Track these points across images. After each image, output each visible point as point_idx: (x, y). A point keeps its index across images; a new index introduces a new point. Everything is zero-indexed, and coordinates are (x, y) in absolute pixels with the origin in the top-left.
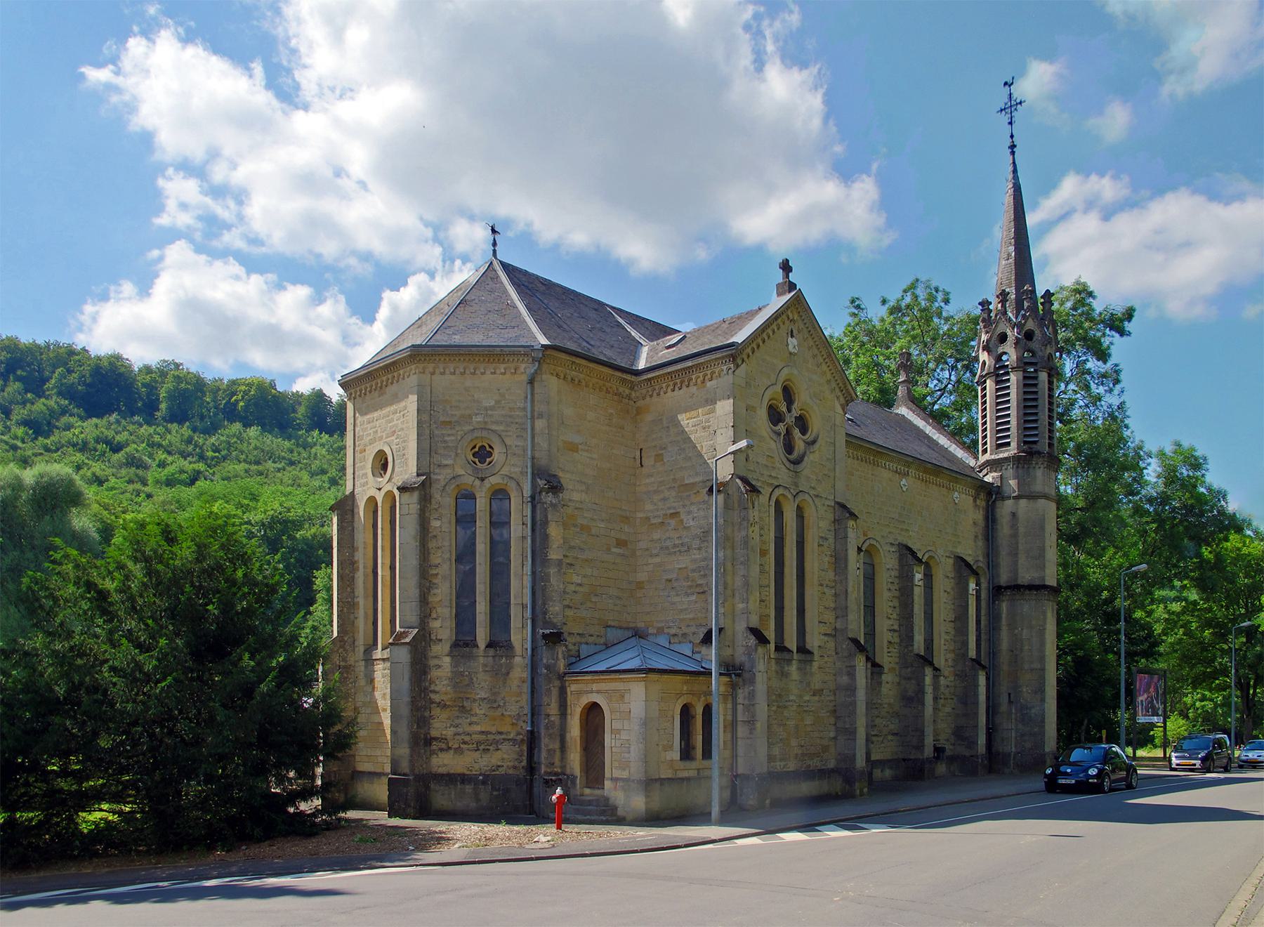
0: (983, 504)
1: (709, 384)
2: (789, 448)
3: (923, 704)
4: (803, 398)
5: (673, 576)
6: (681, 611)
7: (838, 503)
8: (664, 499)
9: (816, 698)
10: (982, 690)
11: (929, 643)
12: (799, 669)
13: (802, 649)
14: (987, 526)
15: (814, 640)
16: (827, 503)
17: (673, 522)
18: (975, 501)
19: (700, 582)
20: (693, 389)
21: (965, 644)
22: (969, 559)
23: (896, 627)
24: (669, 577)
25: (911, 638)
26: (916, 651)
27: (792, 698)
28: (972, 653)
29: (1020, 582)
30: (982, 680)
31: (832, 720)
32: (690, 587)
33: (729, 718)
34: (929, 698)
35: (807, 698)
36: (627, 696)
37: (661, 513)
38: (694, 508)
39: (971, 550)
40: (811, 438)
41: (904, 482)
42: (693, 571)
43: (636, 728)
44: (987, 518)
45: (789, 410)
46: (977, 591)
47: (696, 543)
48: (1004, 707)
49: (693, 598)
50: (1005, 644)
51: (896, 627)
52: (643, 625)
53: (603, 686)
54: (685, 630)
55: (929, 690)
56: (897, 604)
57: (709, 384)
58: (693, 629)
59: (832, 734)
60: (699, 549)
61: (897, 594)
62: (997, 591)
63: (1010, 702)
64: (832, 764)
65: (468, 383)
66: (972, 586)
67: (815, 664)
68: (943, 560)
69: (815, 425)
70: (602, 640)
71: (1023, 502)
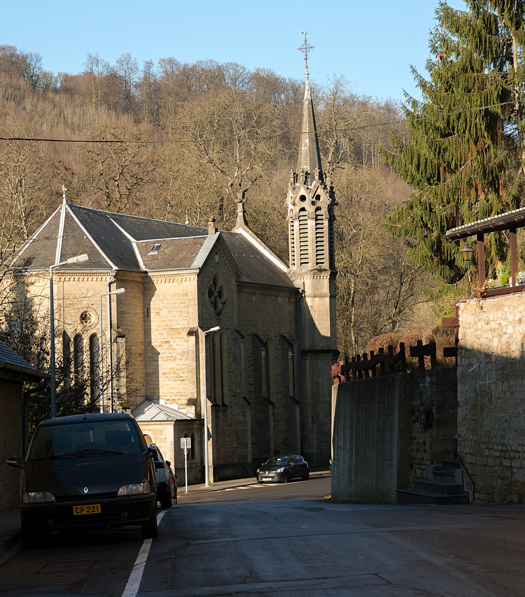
0: (294, 300)
1: (184, 283)
2: (215, 308)
3: (269, 427)
4: (221, 282)
5: (167, 371)
6: (172, 388)
7: (236, 330)
8: (161, 334)
9: (229, 428)
10: (298, 416)
11: (268, 391)
12: (223, 414)
13: (224, 405)
14: (296, 314)
15: (227, 402)
16: (231, 331)
17: (166, 346)
18: (289, 300)
19: (181, 375)
20: (176, 284)
21: (287, 388)
22: (287, 336)
23: (252, 382)
24: (165, 372)
25: (261, 389)
26: (264, 396)
27: (220, 428)
28: (291, 394)
29: (316, 349)
30: (298, 410)
31: (236, 438)
32: (176, 377)
33: (200, 439)
34: (271, 423)
35: (226, 428)
36: (164, 432)
37: (159, 340)
38: (177, 340)
39: (287, 330)
40: (224, 301)
41: (254, 298)
42: (178, 370)
43: (169, 446)
44: (296, 308)
45: (215, 289)
46: (293, 356)
47: (179, 357)
48: (309, 425)
49: (178, 382)
50: (309, 386)
51: (252, 382)
52: (150, 394)
53: (150, 427)
54: (175, 398)
55: (271, 418)
56: (252, 369)
57: (184, 283)
58: (178, 397)
59: (236, 446)
60: (181, 359)
61: (252, 363)
62: (304, 353)
63: (313, 422)
64: (236, 461)
65: (80, 286)
66: (290, 354)
67: (229, 411)
68: (274, 339)
69: (225, 294)
70: (135, 403)
71: (317, 299)
